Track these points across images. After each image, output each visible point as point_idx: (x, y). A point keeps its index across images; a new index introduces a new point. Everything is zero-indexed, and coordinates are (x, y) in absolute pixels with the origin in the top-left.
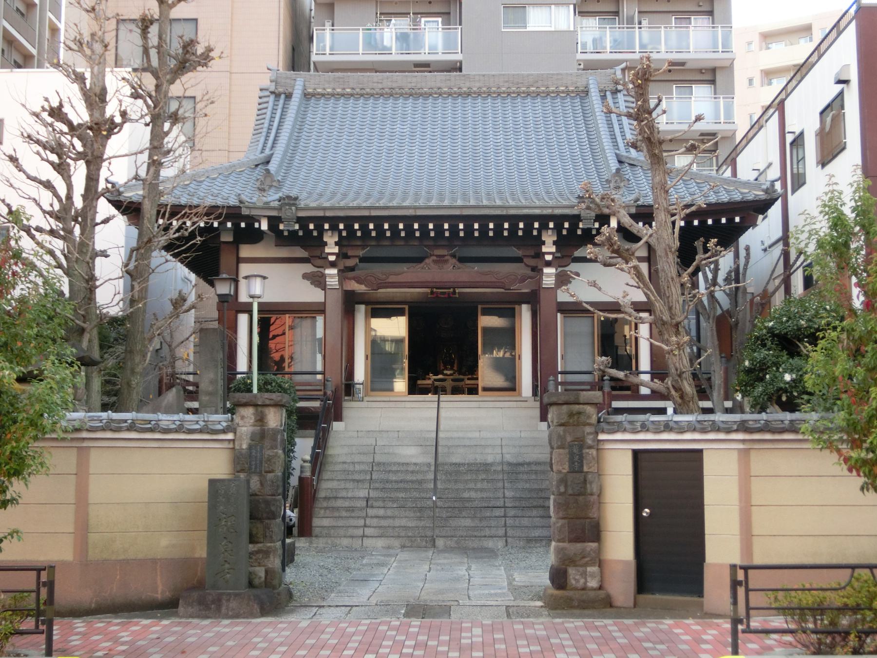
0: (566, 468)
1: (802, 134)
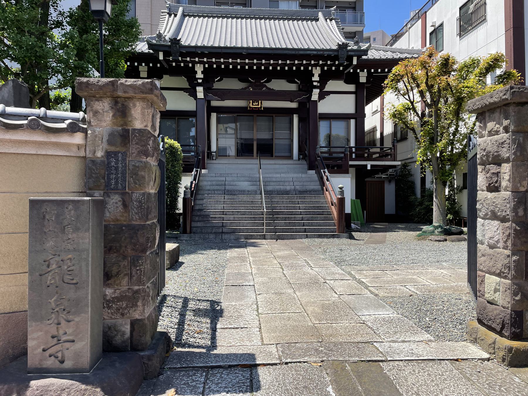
1: (442, 25)
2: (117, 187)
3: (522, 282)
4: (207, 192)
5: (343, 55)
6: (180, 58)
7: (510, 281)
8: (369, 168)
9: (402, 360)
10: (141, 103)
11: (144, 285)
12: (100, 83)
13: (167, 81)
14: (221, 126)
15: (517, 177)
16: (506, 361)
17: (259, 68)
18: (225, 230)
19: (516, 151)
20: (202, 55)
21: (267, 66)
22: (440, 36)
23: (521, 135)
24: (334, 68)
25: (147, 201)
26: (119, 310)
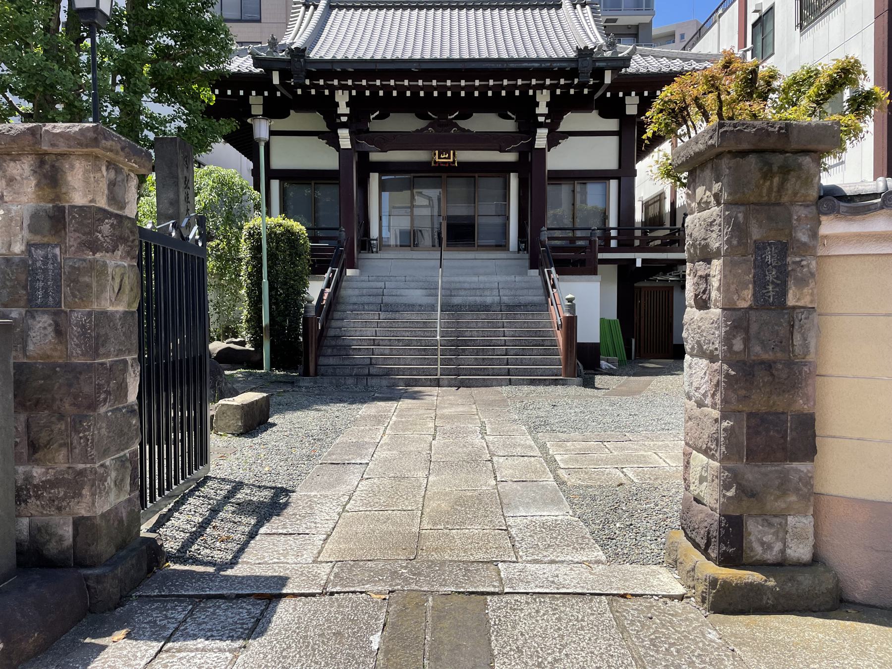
0: (746, 299)
1: (771, 9)
2: (47, 303)
3: (741, 466)
4: (351, 307)
5: (586, 66)
6: (307, 82)
7: (718, 464)
8: (639, 264)
9: (527, 593)
10: (84, 163)
11: (93, 461)
12: (12, 132)
13: (295, 120)
14: (386, 195)
15: (733, 283)
16: (707, 601)
17: (442, 94)
18: (373, 371)
19: (731, 238)
20: (343, 75)
21: (456, 90)
22: (768, 28)
23: (742, 208)
24: (572, 92)
25: (96, 325)
26: (54, 501)
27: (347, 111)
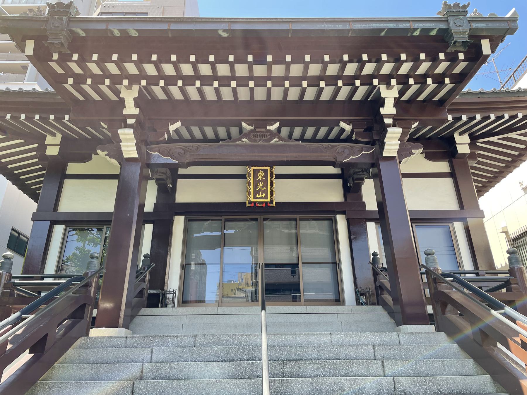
27: (136, 111)
